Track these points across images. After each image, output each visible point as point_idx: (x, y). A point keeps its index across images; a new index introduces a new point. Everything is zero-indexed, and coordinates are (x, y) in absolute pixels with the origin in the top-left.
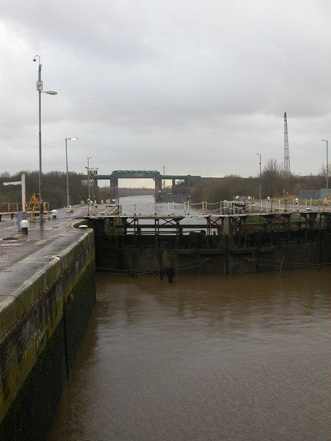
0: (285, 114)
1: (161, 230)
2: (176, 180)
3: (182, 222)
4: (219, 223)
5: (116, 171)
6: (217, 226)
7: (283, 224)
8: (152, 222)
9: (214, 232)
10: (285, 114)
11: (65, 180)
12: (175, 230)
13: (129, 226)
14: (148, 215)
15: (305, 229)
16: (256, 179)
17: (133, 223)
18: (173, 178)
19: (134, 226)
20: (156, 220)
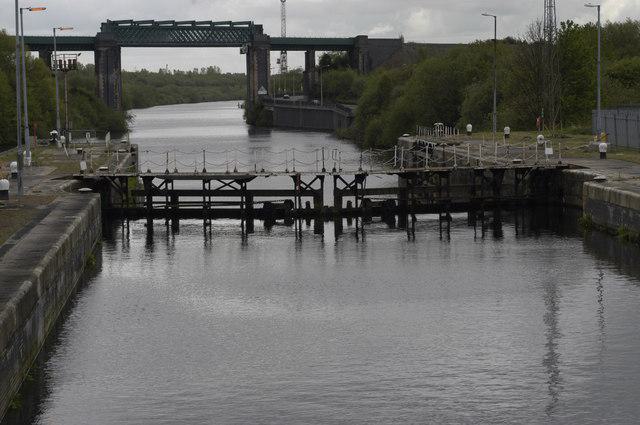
1: (214, 199)
2: (319, 54)
3: (250, 186)
4: (316, 186)
5: (115, 23)
6: (312, 193)
7: (439, 190)
8: (197, 185)
9: (308, 204)
12: (238, 199)
13: (157, 192)
14: (191, 171)
15: (482, 199)
17: (164, 187)
18: (308, 46)
19: (166, 193)
20: (204, 182)
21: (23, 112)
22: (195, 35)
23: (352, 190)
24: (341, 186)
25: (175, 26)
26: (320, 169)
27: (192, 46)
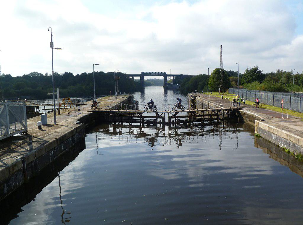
0: (221, 46)
3: (143, 115)
4: (163, 115)
10: (221, 46)
11: (52, 78)
16: (21, 77)
21: (116, 88)
22: (156, 74)
23: (174, 117)
24: (171, 115)
25: (150, 73)
26: (164, 111)
27: (150, 76)
